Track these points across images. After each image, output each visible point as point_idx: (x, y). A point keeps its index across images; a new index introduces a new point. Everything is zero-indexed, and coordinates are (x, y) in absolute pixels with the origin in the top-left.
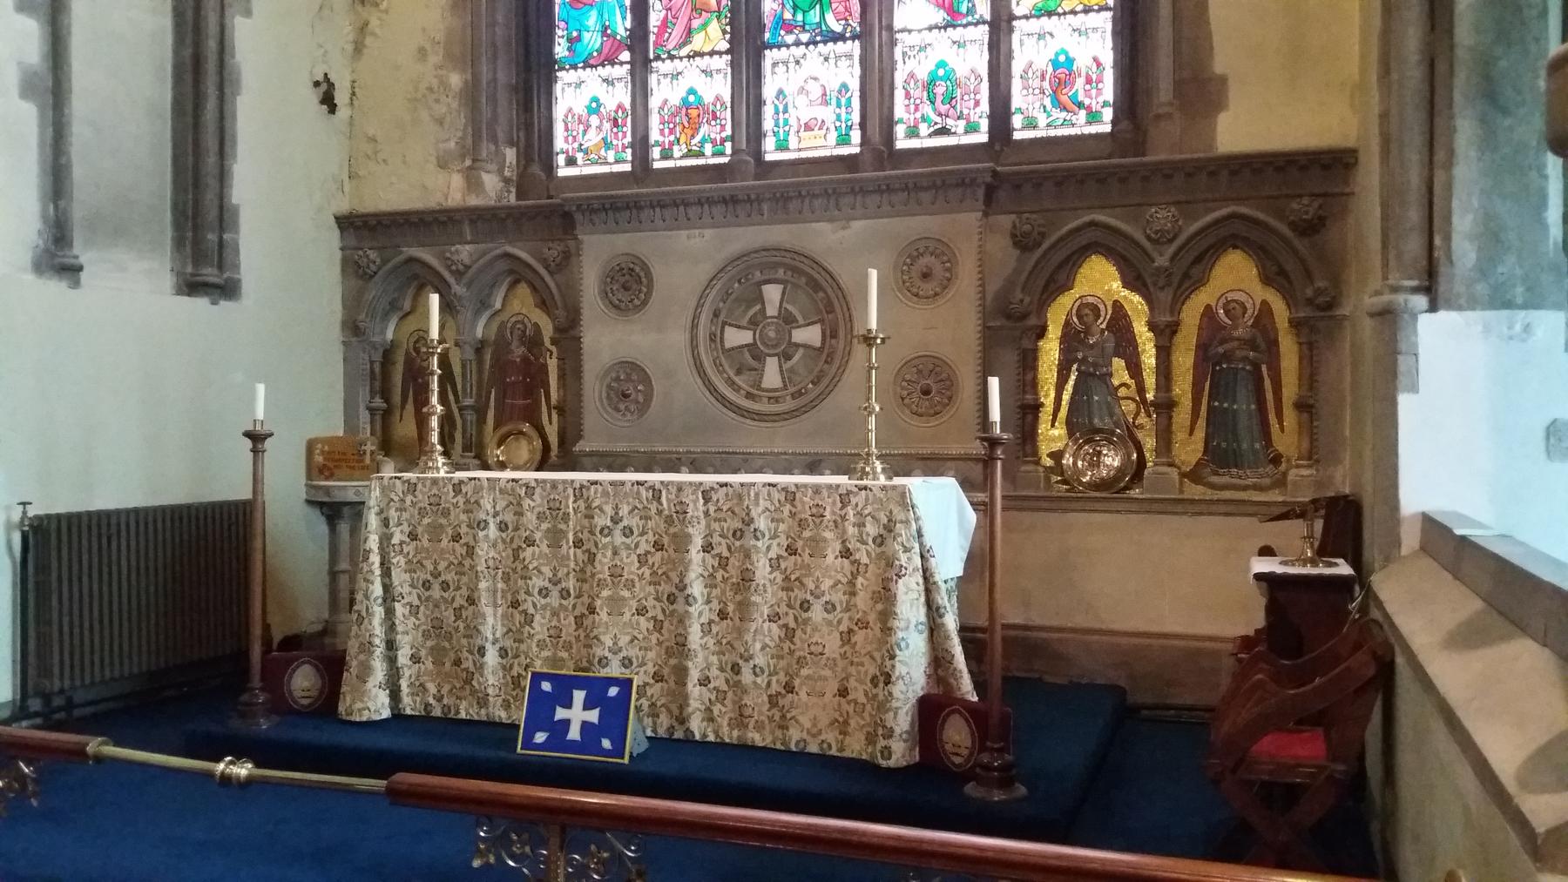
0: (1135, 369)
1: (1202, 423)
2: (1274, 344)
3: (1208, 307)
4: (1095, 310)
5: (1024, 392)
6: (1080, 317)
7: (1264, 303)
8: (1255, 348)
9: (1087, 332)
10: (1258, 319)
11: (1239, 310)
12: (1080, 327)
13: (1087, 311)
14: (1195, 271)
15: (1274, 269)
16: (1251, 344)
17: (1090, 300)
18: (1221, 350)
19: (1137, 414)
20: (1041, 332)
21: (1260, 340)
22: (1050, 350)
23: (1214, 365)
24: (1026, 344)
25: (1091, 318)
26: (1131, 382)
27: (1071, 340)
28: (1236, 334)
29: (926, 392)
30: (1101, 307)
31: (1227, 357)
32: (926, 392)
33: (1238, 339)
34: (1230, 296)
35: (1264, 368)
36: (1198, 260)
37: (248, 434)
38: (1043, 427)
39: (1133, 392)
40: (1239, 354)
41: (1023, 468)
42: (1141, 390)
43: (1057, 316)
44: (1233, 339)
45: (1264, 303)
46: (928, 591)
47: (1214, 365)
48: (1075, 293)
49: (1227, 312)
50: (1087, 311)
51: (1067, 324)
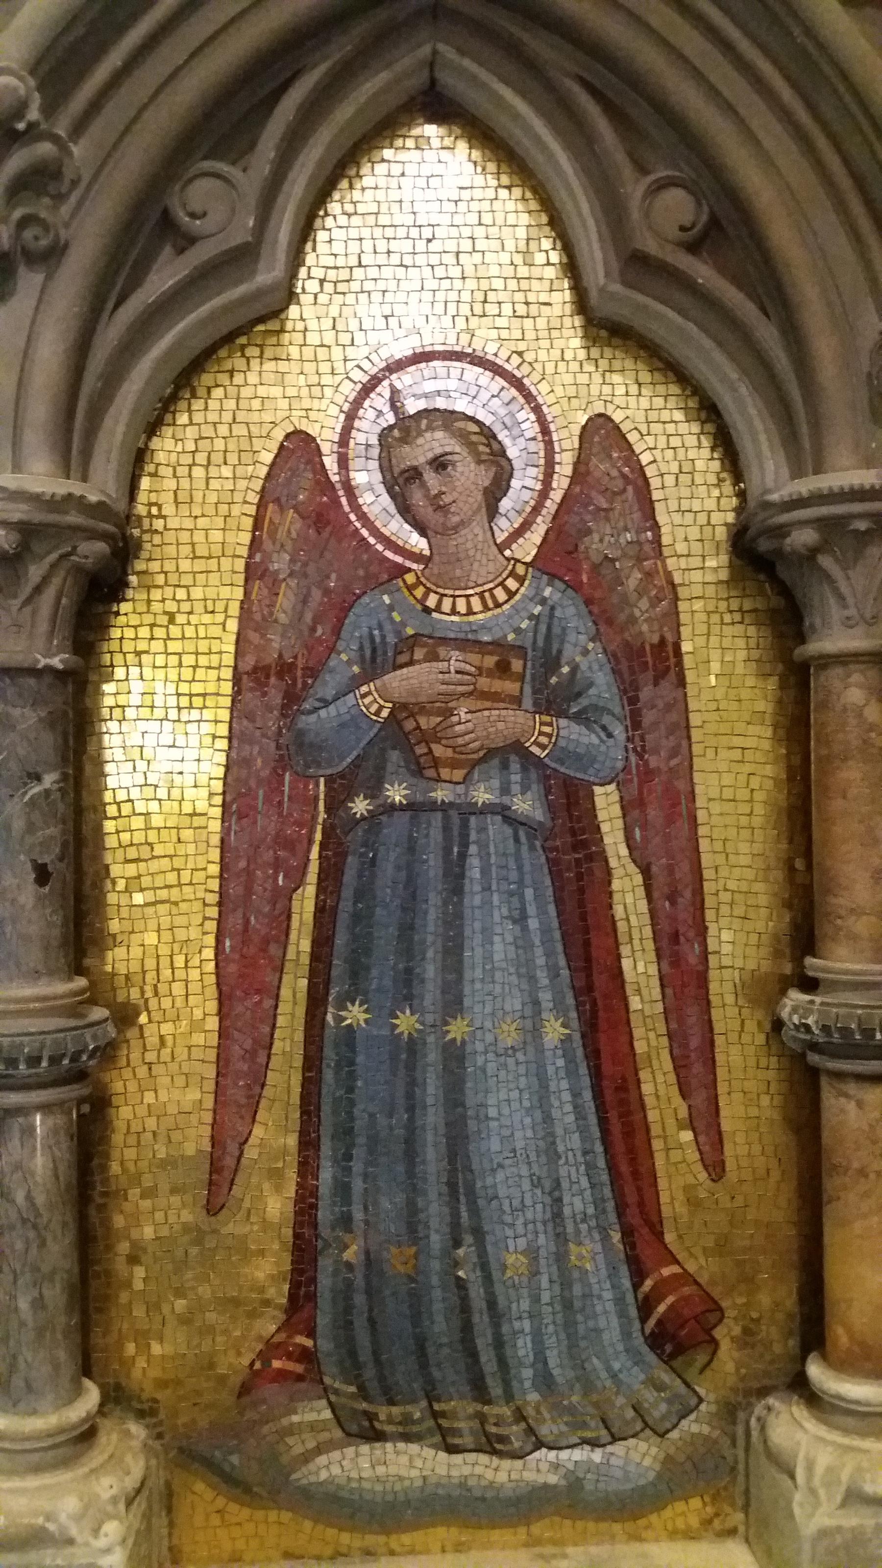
1: (272, 1134)
2: (653, 664)
3: (299, 447)
7: (602, 433)
8: (557, 699)
10: (560, 557)
11: (469, 475)
14: (214, 203)
15: (677, 208)
16: (533, 670)
18: (372, 701)
21: (585, 657)
23: (341, 790)
28: (453, 612)
31: (405, 736)
33: (466, 643)
34: (420, 389)
35: (607, 803)
36: (226, 123)
37: (876, 841)
40: (474, 725)
43: (201, 487)
44: (434, 644)
45: (602, 433)
47: (341, 790)
49: (401, 483)
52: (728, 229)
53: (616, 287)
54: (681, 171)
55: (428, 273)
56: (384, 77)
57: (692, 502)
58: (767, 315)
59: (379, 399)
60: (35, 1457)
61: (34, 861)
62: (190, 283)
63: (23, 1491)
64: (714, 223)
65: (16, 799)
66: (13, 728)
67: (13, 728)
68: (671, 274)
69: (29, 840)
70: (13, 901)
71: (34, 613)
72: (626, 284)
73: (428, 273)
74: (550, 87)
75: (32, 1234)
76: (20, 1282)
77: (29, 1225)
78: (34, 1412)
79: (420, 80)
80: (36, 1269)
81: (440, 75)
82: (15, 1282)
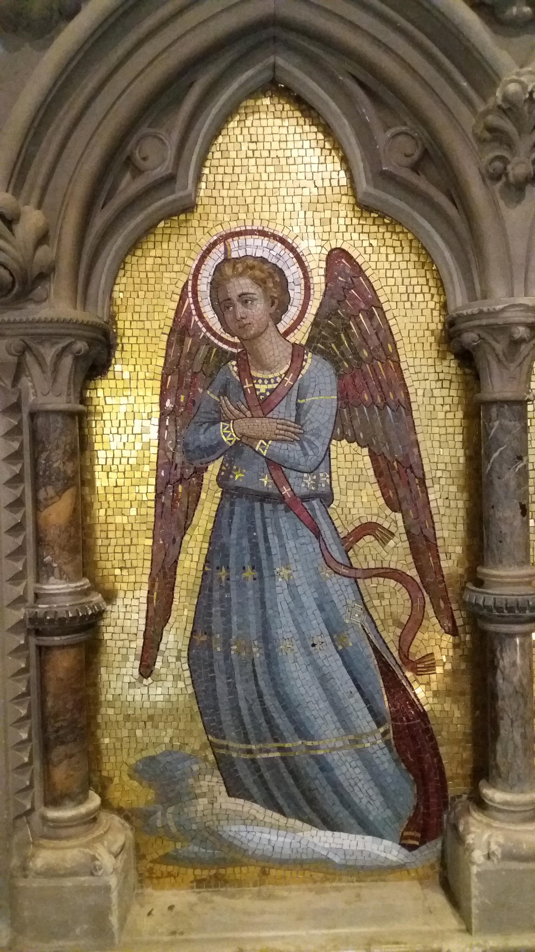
0: (399, 477)
4: (271, 279)
5: (43, 570)
6: (221, 305)
9: (247, 357)
12: (228, 343)
13: (243, 285)
17: (256, 247)
19: (412, 626)
20: (96, 354)
22: (128, 423)
24: (46, 392)
25: (259, 310)
26: (394, 521)
27: (195, 375)
29: (314, 645)
30: (293, 273)
32: (314, 645)
38: (119, 678)
39: (397, 553)
41: (44, 857)
42: (423, 545)
43: (148, 296)
46: (433, 90)
48: (200, 232)
50: (243, 285)
51: (181, 330)
52: (432, 158)
53: (371, 190)
54: (405, 124)
55: (279, 180)
56: (250, 73)
57: (409, 307)
58: (454, 204)
59: (221, 247)
60: (521, 816)
61: (520, 503)
62: (136, 186)
63: (526, 832)
64: (425, 153)
65: (512, 470)
66: (510, 432)
67: (510, 432)
68: (413, 181)
69: (518, 492)
70: (511, 524)
71: (521, 370)
72: (376, 187)
73: (279, 180)
74: (333, 79)
75: (521, 700)
76: (515, 724)
77: (520, 695)
78: (522, 792)
79: (267, 75)
80: (522, 718)
81: (278, 73)
82: (512, 726)
